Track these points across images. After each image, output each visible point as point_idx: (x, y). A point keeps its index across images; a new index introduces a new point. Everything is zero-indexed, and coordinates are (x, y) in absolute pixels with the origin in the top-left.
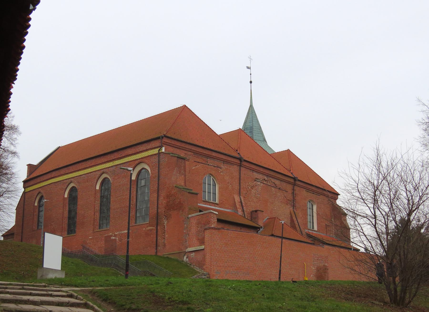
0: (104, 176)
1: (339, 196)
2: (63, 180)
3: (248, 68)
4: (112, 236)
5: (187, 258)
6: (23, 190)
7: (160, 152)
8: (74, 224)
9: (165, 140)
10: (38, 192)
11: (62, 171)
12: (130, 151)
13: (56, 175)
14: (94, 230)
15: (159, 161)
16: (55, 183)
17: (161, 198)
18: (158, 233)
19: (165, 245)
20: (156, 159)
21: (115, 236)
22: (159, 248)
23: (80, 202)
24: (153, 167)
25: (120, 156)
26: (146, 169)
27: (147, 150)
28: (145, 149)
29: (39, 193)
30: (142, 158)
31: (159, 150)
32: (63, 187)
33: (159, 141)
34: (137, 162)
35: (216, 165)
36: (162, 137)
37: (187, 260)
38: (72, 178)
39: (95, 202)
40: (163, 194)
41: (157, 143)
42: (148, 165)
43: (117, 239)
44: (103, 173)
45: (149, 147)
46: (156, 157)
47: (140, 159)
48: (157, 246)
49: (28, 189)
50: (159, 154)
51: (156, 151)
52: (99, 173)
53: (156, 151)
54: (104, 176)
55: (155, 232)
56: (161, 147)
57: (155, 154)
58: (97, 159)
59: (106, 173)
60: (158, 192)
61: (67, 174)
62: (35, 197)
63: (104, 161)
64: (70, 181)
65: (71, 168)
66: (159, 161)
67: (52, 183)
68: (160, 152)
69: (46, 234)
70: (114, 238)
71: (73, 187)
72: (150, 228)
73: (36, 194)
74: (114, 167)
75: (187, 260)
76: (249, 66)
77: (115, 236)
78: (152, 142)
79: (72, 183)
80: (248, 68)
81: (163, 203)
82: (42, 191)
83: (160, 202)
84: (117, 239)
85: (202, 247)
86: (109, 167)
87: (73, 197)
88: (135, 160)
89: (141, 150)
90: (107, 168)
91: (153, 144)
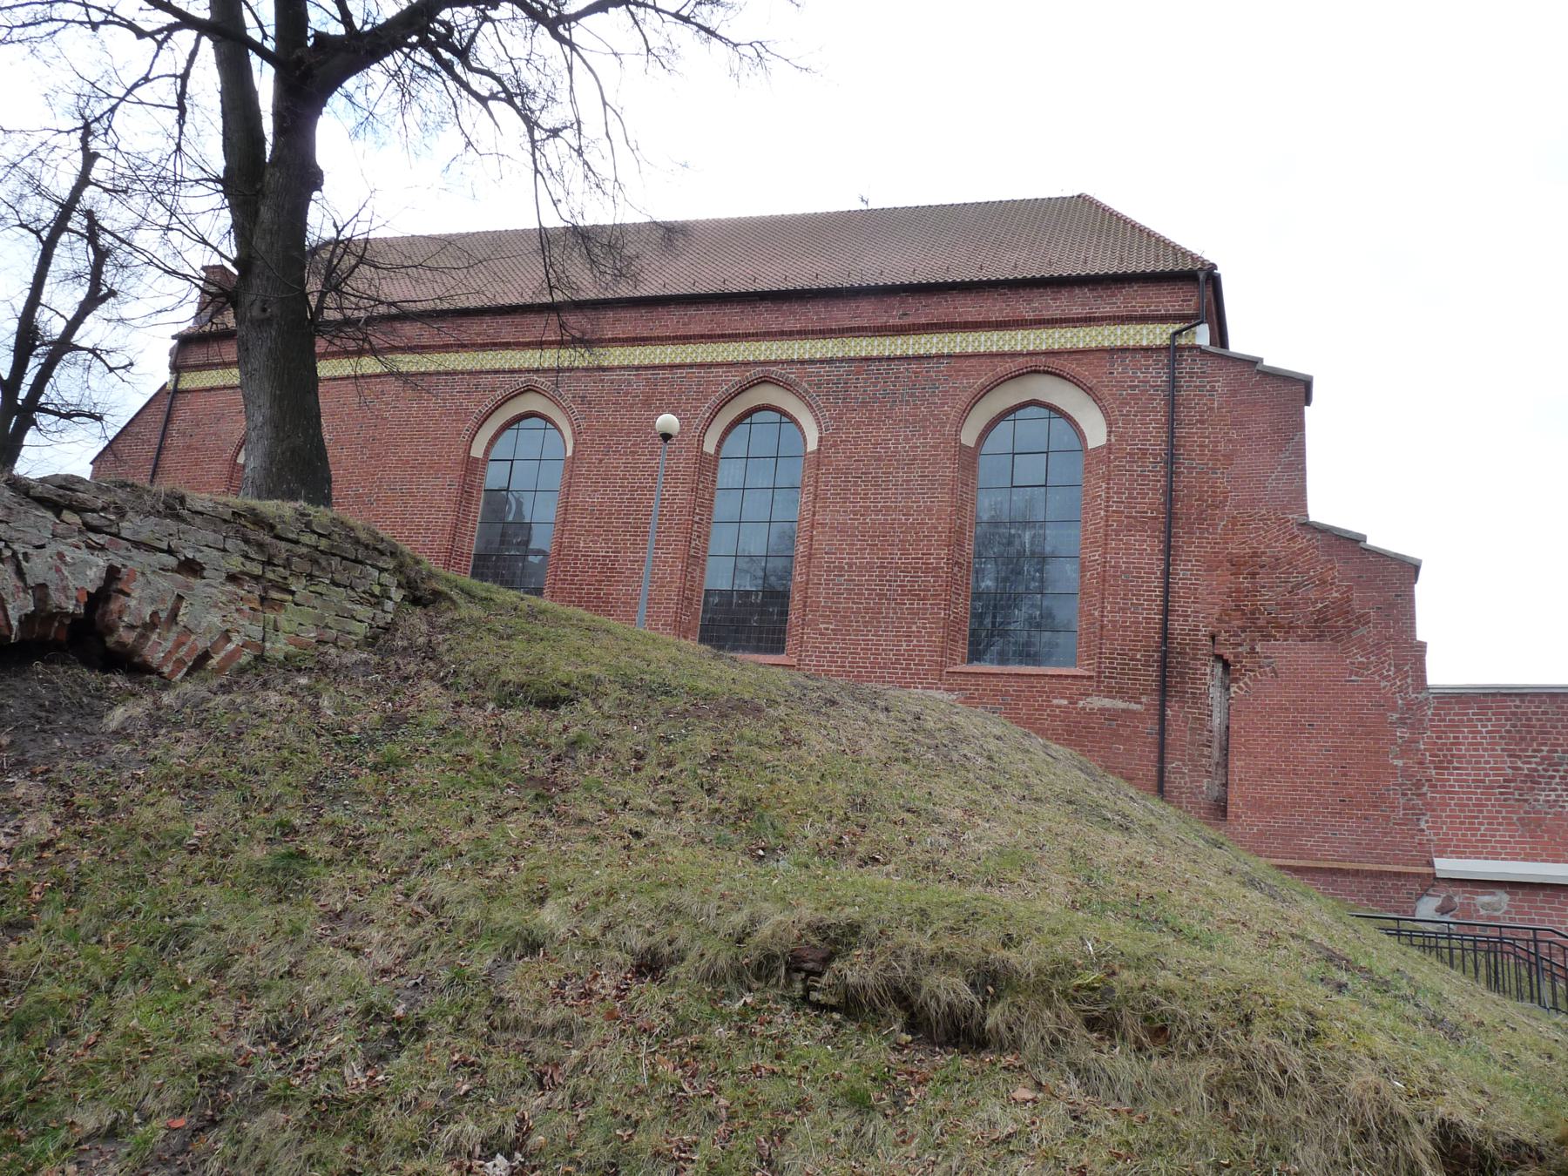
6: (163, 376)
7: (1183, 341)
12: (969, 308)
25: (897, 321)
26: (547, 419)
27: (1088, 321)
28: (1077, 311)
30: (1051, 353)
32: (471, 406)
34: (1012, 366)
44: (529, 389)
45: (1107, 310)
47: (1030, 354)
49: (191, 381)
50: (1173, 351)
51: (1157, 335)
52: (735, 377)
53: (1157, 335)
59: (787, 386)
63: (775, 327)
69: (88, 478)
72: (1107, 703)
73: (965, 397)
75: (1144, 699)
76: (133, 369)
79: (530, 396)
83: (1178, 586)
86: (812, 362)
88: (1001, 355)
89: (1047, 314)
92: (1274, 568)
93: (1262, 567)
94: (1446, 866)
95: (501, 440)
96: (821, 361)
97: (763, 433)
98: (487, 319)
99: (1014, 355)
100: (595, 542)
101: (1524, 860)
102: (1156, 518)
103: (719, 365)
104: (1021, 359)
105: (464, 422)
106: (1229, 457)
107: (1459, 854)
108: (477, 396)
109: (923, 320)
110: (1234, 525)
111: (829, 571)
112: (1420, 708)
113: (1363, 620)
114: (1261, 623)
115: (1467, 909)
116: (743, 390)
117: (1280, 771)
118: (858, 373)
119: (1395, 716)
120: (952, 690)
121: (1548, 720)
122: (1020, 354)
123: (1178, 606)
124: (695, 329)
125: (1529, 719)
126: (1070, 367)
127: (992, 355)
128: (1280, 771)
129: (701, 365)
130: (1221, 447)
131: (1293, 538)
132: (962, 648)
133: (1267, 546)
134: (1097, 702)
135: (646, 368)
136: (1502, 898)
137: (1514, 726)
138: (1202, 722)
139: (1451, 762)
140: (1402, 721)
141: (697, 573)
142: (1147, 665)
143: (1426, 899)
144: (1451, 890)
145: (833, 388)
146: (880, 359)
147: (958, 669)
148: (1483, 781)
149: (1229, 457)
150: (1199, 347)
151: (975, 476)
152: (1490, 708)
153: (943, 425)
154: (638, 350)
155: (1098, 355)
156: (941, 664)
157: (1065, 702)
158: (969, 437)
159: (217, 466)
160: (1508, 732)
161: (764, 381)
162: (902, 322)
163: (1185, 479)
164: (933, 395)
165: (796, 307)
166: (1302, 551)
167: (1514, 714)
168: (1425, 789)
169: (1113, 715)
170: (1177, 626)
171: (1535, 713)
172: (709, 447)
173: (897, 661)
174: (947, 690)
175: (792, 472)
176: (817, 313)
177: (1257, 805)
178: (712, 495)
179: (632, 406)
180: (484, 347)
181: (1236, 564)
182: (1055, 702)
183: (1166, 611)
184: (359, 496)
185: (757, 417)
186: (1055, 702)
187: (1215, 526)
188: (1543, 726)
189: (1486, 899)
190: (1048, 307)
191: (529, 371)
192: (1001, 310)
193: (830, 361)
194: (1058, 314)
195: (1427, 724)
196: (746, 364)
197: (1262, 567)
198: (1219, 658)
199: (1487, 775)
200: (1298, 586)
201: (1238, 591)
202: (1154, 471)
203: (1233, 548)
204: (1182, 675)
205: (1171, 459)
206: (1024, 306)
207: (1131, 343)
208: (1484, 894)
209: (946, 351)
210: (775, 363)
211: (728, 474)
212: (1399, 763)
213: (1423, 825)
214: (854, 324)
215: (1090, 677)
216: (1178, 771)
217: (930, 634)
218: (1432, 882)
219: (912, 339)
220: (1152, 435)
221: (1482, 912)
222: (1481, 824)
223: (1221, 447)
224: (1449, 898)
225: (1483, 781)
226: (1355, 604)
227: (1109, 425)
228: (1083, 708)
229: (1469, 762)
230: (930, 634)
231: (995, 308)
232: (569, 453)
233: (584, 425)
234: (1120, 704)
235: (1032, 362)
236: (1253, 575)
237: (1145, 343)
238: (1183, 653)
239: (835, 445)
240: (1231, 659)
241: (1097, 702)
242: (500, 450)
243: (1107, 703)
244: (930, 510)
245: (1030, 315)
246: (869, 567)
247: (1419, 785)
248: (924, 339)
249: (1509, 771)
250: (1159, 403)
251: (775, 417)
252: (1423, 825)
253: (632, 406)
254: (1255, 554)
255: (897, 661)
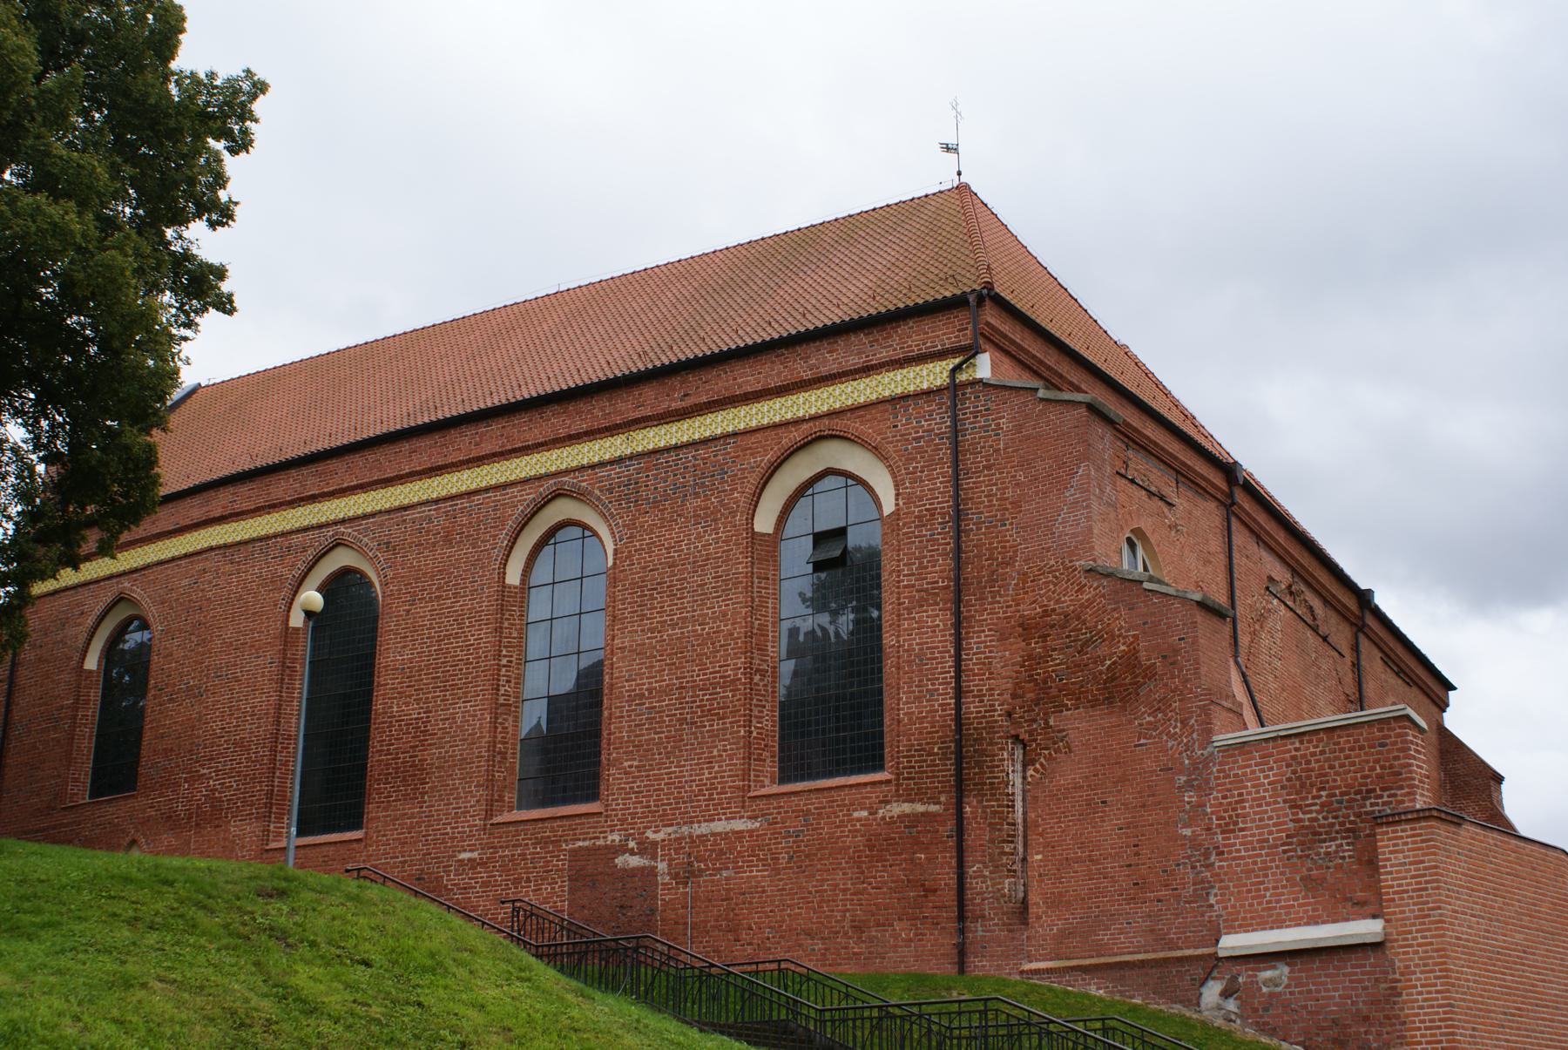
0: (563, 510)
1: (1451, 693)
2: (283, 534)
3: (947, 148)
4: (622, 849)
5: (1226, 994)
7: (963, 377)
8: (359, 771)
9: (991, 316)
10: (108, 598)
11: (281, 487)
12: (747, 377)
13: (238, 507)
14: (489, 813)
15: (956, 431)
16: (226, 546)
17: (979, 642)
18: (970, 839)
19: (1022, 911)
20: (939, 422)
21: (647, 848)
22: (977, 931)
23: (393, 654)
24: (910, 460)
25: (674, 405)
26: (585, 527)
27: (867, 370)
28: (855, 361)
29: (120, 600)
30: (832, 414)
31: (956, 370)
32: (285, 571)
33: (960, 318)
34: (796, 435)
35: (1153, 489)
36: (981, 300)
37: (1231, 1005)
38: (343, 521)
39: (499, 656)
40: (986, 619)
41: (944, 332)
42: (876, 450)
43: (662, 866)
44: (337, 544)
45: (883, 355)
46: (946, 399)
48: (961, 917)
50: (954, 390)
51: (934, 375)
53: (934, 375)
54: (341, 559)
55: (951, 825)
56: (969, 353)
57: (928, 393)
58: (522, 419)
59: (578, 495)
60: (958, 601)
61: (313, 499)
62: (90, 622)
63: (562, 432)
64: (334, 537)
65: (463, 443)
66: (956, 431)
67: (211, 549)
68: (963, 377)
70: (635, 861)
71: (346, 572)
72: (907, 808)
73: (753, 479)
74: (635, 465)
76: (952, 141)
77: (647, 848)
78: (903, 329)
80: (947, 148)
81: (997, 665)
82: (137, 593)
83: (971, 662)
84: (662, 866)
85: (1367, 929)
86: (602, 464)
87: (349, 620)
88: (785, 424)
89: (824, 370)
90: (581, 468)
91: (913, 337)
92: (1063, 627)
93: (1052, 626)
94: (1233, 943)
95: (796, 512)
96: (611, 462)
97: (566, 556)
98: (293, 472)
99: (797, 422)
100: (407, 704)
101: (1307, 924)
102: (947, 587)
103: (513, 484)
104: (805, 426)
105: (280, 590)
106: (1016, 504)
107: (1246, 927)
108: (289, 560)
109: (704, 399)
110: (1025, 582)
111: (630, 701)
112: (1206, 766)
113: (1150, 673)
114: (1054, 692)
115: (1253, 985)
116: (539, 508)
117: (1077, 860)
118: (648, 469)
119: (1183, 778)
120: (754, 818)
121: (1327, 760)
122: (802, 421)
123: (972, 684)
124: (487, 448)
125: (1308, 762)
126: (854, 426)
127: (776, 426)
128: (1077, 860)
129: (496, 488)
130: (1009, 493)
131: (1080, 590)
132: (771, 767)
133: (1058, 602)
134: (898, 809)
135: (445, 499)
136: (1282, 971)
137: (1294, 772)
138: (1001, 816)
139: (1236, 823)
140: (1189, 784)
141: (509, 723)
142: (944, 758)
143: (1210, 983)
144: (1236, 969)
145: (626, 488)
146: (667, 449)
147: (763, 791)
148: (1267, 840)
149: (1016, 504)
150: (981, 381)
151: (777, 567)
152: (1271, 755)
153: (733, 513)
154: (436, 481)
155: (880, 407)
156: (742, 789)
157: (865, 813)
158: (764, 522)
159: (65, 676)
160: (1289, 780)
161: (557, 495)
162: (684, 404)
163: (975, 536)
164: (723, 481)
165: (581, 405)
166: (1090, 602)
167: (1294, 758)
168: (1213, 858)
169: (913, 820)
170: (972, 707)
171: (1313, 754)
172: (513, 577)
173: (701, 793)
174: (750, 818)
175: (597, 591)
176: (602, 409)
177: (1056, 902)
178: (520, 631)
179: (434, 544)
180: (292, 504)
181: (1027, 629)
182: (856, 815)
183: (959, 693)
184: (189, 689)
185: (560, 536)
186: (856, 815)
187: (1006, 587)
188: (1322, 768)
189: (1268, 974)
190: (825, 361)
191: (335, 523)
192: (779, 374)
193: (619, 461)
194: (834, 368)
195: (1213, 783)
196: (539, 478)
197: (1052, 626)
198: (1016, 738)
199: (1270, 833)
200: (1087, 643)
201: (1030, 657)
202: (941, 532)
203: (1027, 610)
204: (979, 764)
205: (958, 515)
206: (801, 365)
207: (912, 388)
208: (1265, 969)
209: (730, 429)
210: (567, 472)
211: (539, 607)
212: (1188, 832)
213: (1212, 900)
214: (638, 415)
215: (888, 782)
216: (979, 874)
217: (731, 757)
218: (1214, 964)
219: (698, 421)
220: (937, 486)
221: (1265, 990)
222: (1266, 889)
223: (1009, 493)
224: (1234, 979)
225: (1267, 840)
226: (1142, 654)
227: (897, 486)
228: (883, 818)
229: (1253, 821)
230: (731, 757)
231: (771, 372)
232: (610, 563)
233: (391, 574)
234: (920, 808)
235: (815, 427)
236: (1044, 637)
237: (925, 386)
238: (979, 740)
239: (629, 557)
240: (1027, 737)
241: (898, 809)
242: (542, 573)
243: (907, 808)
244: (725, 615)
245: (807, 375)
246: (666, 691)
247: (1207, 855)
248: (709, 418)
249: (1291, 825)
250: (945, 453)
251: (841, 481)
252: (1212, 900)
253: (434, 544)
254: (1046, 613)
255: (701, 793)
